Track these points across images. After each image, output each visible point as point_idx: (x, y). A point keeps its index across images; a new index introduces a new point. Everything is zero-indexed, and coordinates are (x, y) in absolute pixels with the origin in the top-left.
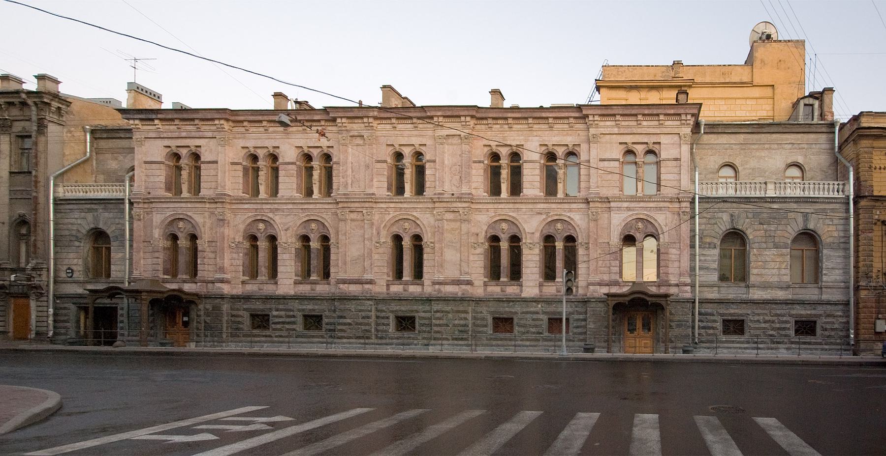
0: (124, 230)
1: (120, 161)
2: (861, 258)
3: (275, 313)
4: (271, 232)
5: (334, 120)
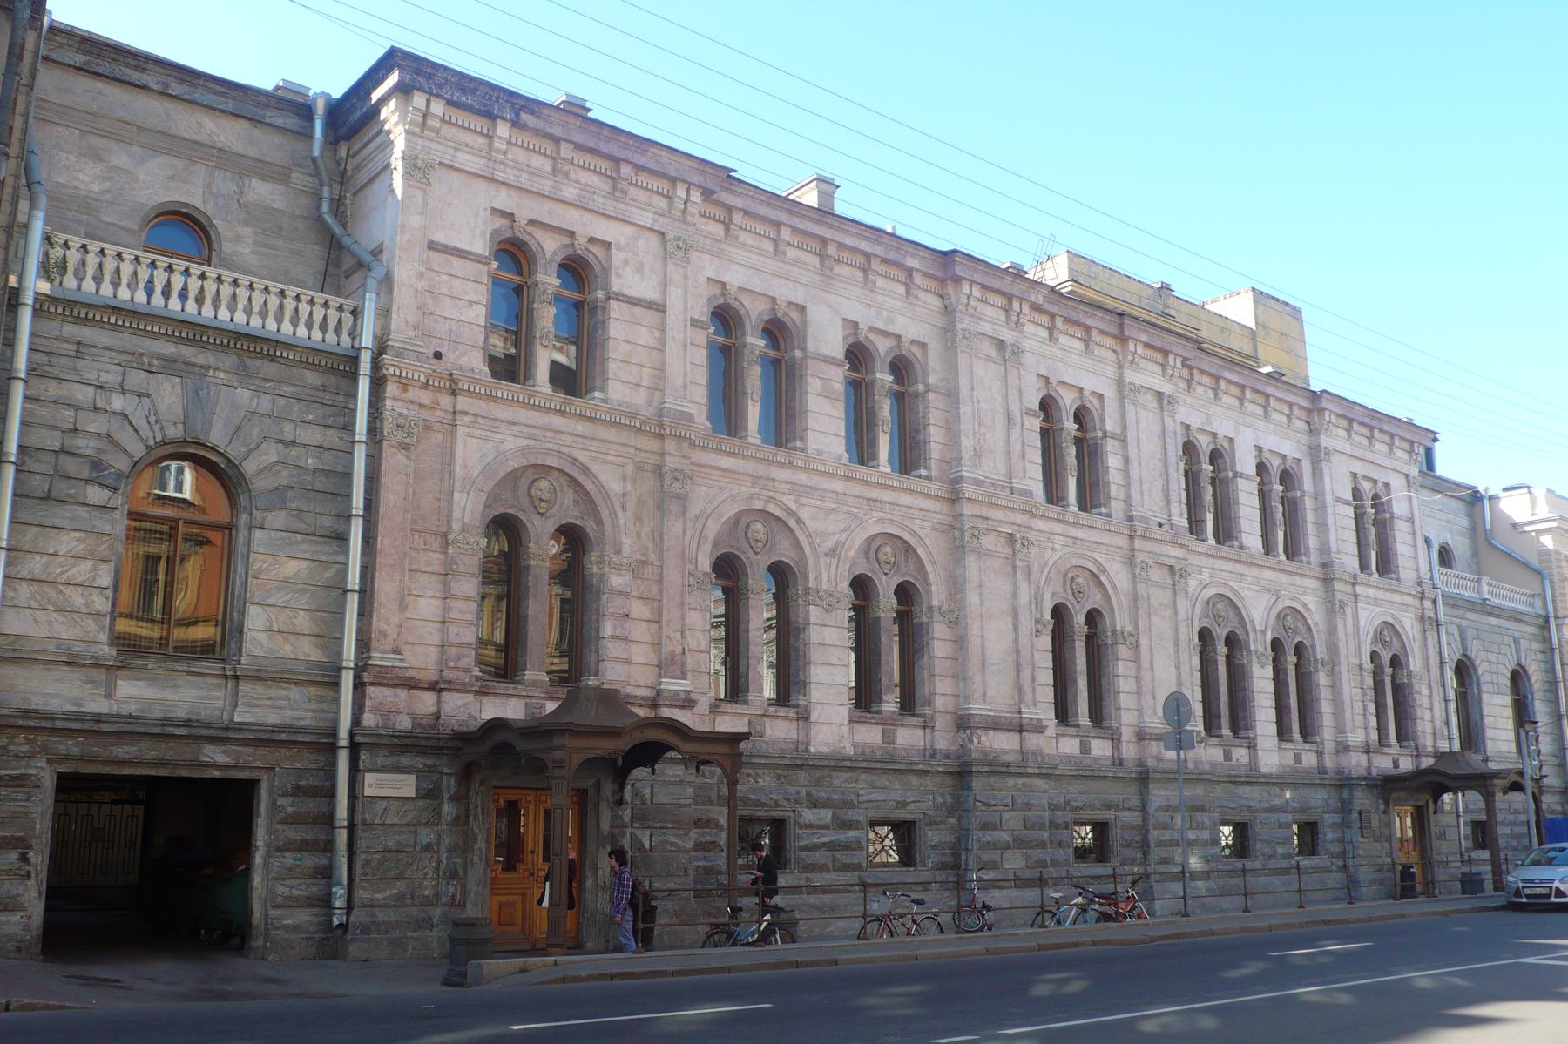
0: (348, 476)
1: (116, 168)
3: (809, 815)
4: (785, 554)
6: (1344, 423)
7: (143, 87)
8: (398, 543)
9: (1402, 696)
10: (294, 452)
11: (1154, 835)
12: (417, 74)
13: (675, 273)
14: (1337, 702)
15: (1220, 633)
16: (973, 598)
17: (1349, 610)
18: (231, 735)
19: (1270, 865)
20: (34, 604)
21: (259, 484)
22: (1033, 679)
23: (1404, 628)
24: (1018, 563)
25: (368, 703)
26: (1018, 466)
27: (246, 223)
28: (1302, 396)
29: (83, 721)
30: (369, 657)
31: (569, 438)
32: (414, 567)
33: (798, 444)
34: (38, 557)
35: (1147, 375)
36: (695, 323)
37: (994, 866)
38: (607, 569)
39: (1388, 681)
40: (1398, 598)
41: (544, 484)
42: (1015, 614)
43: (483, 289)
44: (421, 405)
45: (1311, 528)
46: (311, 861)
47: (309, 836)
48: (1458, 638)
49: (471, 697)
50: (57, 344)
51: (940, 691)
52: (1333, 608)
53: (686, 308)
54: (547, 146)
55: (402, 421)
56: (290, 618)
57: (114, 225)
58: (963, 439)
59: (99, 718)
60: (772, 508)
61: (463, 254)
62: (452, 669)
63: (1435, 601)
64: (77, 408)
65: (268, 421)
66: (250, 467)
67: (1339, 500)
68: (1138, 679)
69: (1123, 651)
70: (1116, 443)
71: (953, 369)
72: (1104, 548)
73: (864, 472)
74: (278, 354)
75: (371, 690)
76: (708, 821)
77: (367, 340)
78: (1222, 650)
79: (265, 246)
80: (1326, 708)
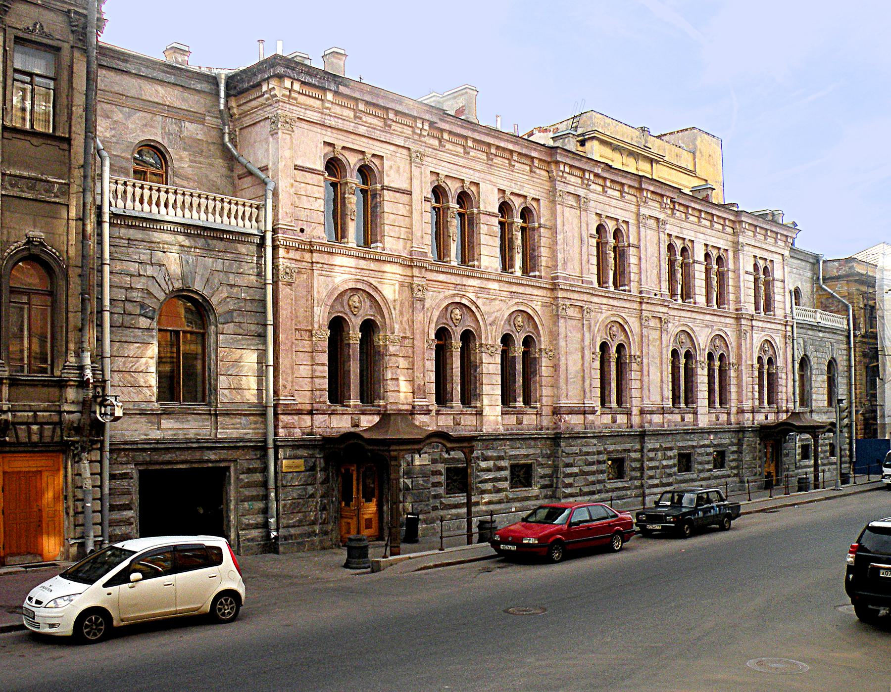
1: (116, 122)
2: (858, 387)
5: (640, 189)
6: (753, 229)
7: (127, 72)
8: (289, 337)
9: (772, 379)
10: (235, 290)
11: (647, 464)
12: (288, 68)
13: (416, 171)
14: (739, 385)
15: (453, 188)
16: (562, 343)
17: (748, 335)
18: (218, 445)
19: (702, 475)
20: (121, 384)
21: (219, 310)
22: (591, 385)
23: (776, 343)
24: (585, 322)
25: (280, 424)
26: (585, 267)
27: (185, 149)
28: (731, 214)
29: (151, 444)
30: (279, 400)
31: (368, 272)
32: (297, 349)
33: (476, 263)
34: (120, 359)
35: (653, 209)
36: (427, 200)
37: (570, 485)
38: (388, 343)
39: (765, 372)
40: (773, 326)
41: (356, 298)
42: (583, 349)
43: (322, 189)
44: (296, 260)
45: (731, 289)
46: (260, 505)
47: (255, 493)
48: (802, 345)
49: (327, 416)
50: (118, 240)
51: (545, 394)
52: (740, 334)
53: (421, 192)
54: (351, 104)
55: (288, 271)
56: (239, 381)
57: (118, 156)
58: (559, 255)
59: (158, 442)
60: (464, 301)
61: (312, 171)
62: (318, 403)
63: (792, 326)
64: (132, 276)
65: (222, 274)
66: (214, 301)
67: (747, 273)
68: (641, 381)
69: (634, 366)
70: (635, 249)
71: (554, 214)
72: (627, 310)
73: (506, 277)
74: (225, 236)
75: (281, 417)
76: (436, 471)
77: (269, 228)
78: (683, 361)
79: (195, 162)
80: (733, 389)
